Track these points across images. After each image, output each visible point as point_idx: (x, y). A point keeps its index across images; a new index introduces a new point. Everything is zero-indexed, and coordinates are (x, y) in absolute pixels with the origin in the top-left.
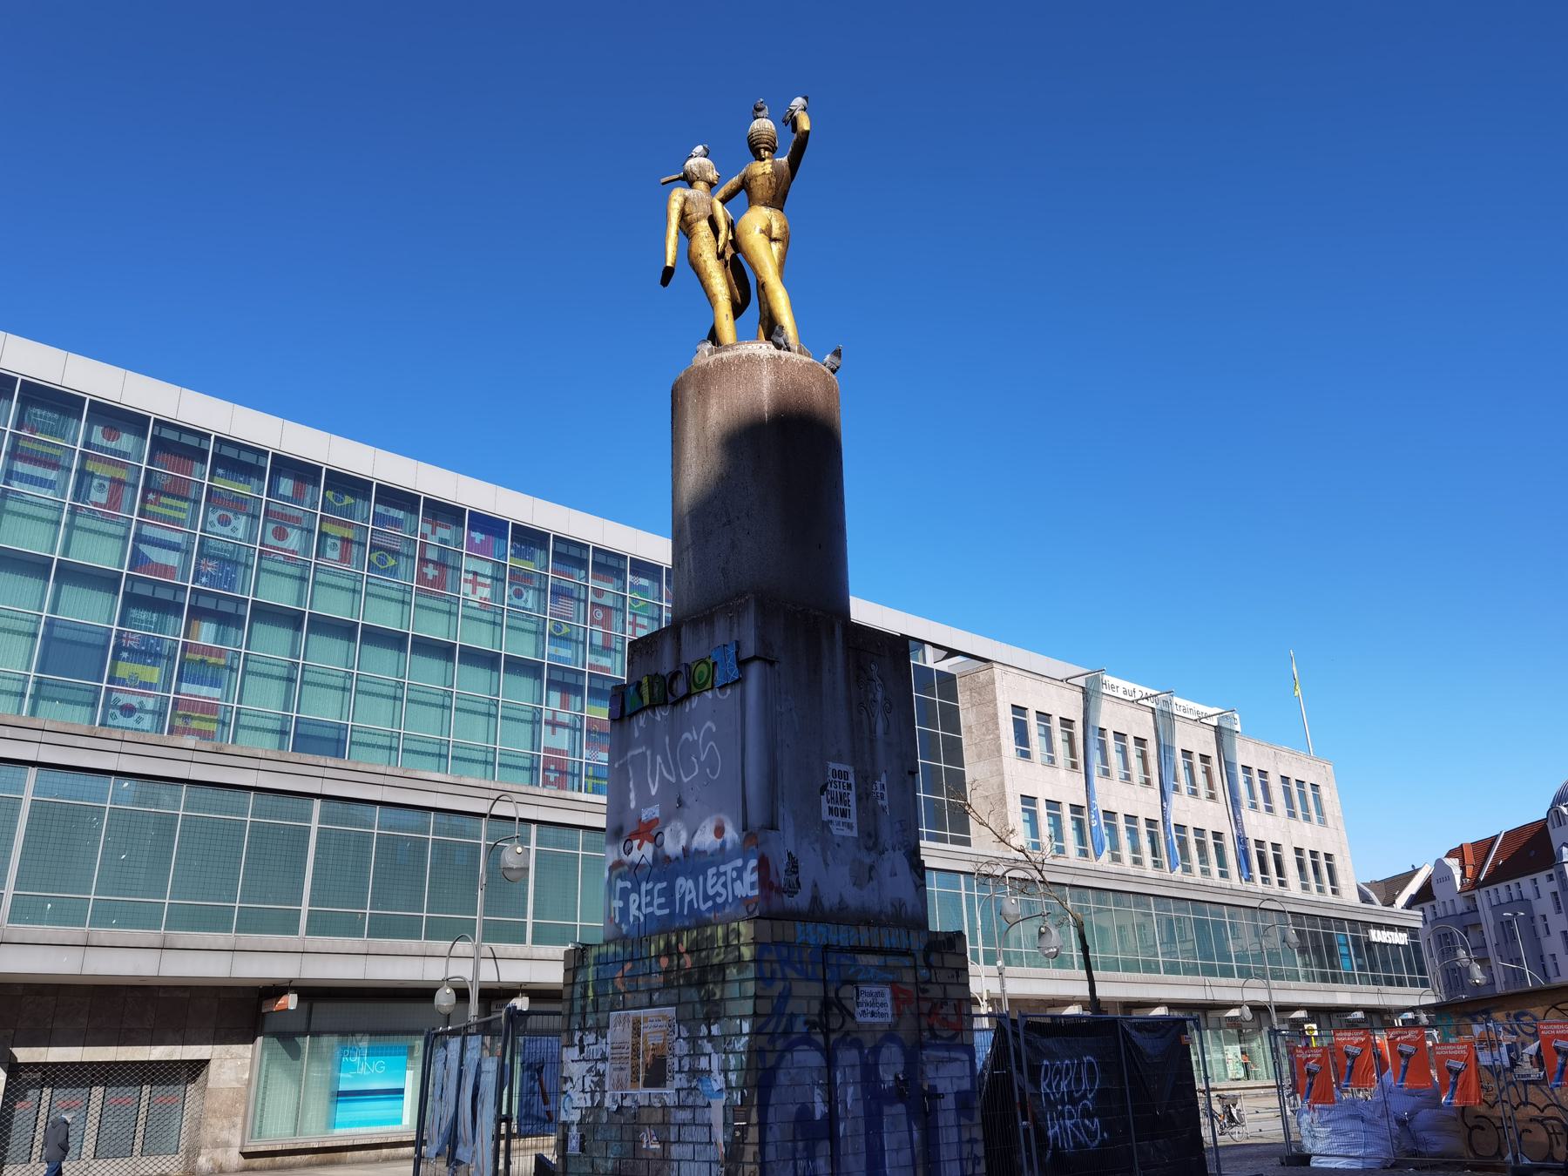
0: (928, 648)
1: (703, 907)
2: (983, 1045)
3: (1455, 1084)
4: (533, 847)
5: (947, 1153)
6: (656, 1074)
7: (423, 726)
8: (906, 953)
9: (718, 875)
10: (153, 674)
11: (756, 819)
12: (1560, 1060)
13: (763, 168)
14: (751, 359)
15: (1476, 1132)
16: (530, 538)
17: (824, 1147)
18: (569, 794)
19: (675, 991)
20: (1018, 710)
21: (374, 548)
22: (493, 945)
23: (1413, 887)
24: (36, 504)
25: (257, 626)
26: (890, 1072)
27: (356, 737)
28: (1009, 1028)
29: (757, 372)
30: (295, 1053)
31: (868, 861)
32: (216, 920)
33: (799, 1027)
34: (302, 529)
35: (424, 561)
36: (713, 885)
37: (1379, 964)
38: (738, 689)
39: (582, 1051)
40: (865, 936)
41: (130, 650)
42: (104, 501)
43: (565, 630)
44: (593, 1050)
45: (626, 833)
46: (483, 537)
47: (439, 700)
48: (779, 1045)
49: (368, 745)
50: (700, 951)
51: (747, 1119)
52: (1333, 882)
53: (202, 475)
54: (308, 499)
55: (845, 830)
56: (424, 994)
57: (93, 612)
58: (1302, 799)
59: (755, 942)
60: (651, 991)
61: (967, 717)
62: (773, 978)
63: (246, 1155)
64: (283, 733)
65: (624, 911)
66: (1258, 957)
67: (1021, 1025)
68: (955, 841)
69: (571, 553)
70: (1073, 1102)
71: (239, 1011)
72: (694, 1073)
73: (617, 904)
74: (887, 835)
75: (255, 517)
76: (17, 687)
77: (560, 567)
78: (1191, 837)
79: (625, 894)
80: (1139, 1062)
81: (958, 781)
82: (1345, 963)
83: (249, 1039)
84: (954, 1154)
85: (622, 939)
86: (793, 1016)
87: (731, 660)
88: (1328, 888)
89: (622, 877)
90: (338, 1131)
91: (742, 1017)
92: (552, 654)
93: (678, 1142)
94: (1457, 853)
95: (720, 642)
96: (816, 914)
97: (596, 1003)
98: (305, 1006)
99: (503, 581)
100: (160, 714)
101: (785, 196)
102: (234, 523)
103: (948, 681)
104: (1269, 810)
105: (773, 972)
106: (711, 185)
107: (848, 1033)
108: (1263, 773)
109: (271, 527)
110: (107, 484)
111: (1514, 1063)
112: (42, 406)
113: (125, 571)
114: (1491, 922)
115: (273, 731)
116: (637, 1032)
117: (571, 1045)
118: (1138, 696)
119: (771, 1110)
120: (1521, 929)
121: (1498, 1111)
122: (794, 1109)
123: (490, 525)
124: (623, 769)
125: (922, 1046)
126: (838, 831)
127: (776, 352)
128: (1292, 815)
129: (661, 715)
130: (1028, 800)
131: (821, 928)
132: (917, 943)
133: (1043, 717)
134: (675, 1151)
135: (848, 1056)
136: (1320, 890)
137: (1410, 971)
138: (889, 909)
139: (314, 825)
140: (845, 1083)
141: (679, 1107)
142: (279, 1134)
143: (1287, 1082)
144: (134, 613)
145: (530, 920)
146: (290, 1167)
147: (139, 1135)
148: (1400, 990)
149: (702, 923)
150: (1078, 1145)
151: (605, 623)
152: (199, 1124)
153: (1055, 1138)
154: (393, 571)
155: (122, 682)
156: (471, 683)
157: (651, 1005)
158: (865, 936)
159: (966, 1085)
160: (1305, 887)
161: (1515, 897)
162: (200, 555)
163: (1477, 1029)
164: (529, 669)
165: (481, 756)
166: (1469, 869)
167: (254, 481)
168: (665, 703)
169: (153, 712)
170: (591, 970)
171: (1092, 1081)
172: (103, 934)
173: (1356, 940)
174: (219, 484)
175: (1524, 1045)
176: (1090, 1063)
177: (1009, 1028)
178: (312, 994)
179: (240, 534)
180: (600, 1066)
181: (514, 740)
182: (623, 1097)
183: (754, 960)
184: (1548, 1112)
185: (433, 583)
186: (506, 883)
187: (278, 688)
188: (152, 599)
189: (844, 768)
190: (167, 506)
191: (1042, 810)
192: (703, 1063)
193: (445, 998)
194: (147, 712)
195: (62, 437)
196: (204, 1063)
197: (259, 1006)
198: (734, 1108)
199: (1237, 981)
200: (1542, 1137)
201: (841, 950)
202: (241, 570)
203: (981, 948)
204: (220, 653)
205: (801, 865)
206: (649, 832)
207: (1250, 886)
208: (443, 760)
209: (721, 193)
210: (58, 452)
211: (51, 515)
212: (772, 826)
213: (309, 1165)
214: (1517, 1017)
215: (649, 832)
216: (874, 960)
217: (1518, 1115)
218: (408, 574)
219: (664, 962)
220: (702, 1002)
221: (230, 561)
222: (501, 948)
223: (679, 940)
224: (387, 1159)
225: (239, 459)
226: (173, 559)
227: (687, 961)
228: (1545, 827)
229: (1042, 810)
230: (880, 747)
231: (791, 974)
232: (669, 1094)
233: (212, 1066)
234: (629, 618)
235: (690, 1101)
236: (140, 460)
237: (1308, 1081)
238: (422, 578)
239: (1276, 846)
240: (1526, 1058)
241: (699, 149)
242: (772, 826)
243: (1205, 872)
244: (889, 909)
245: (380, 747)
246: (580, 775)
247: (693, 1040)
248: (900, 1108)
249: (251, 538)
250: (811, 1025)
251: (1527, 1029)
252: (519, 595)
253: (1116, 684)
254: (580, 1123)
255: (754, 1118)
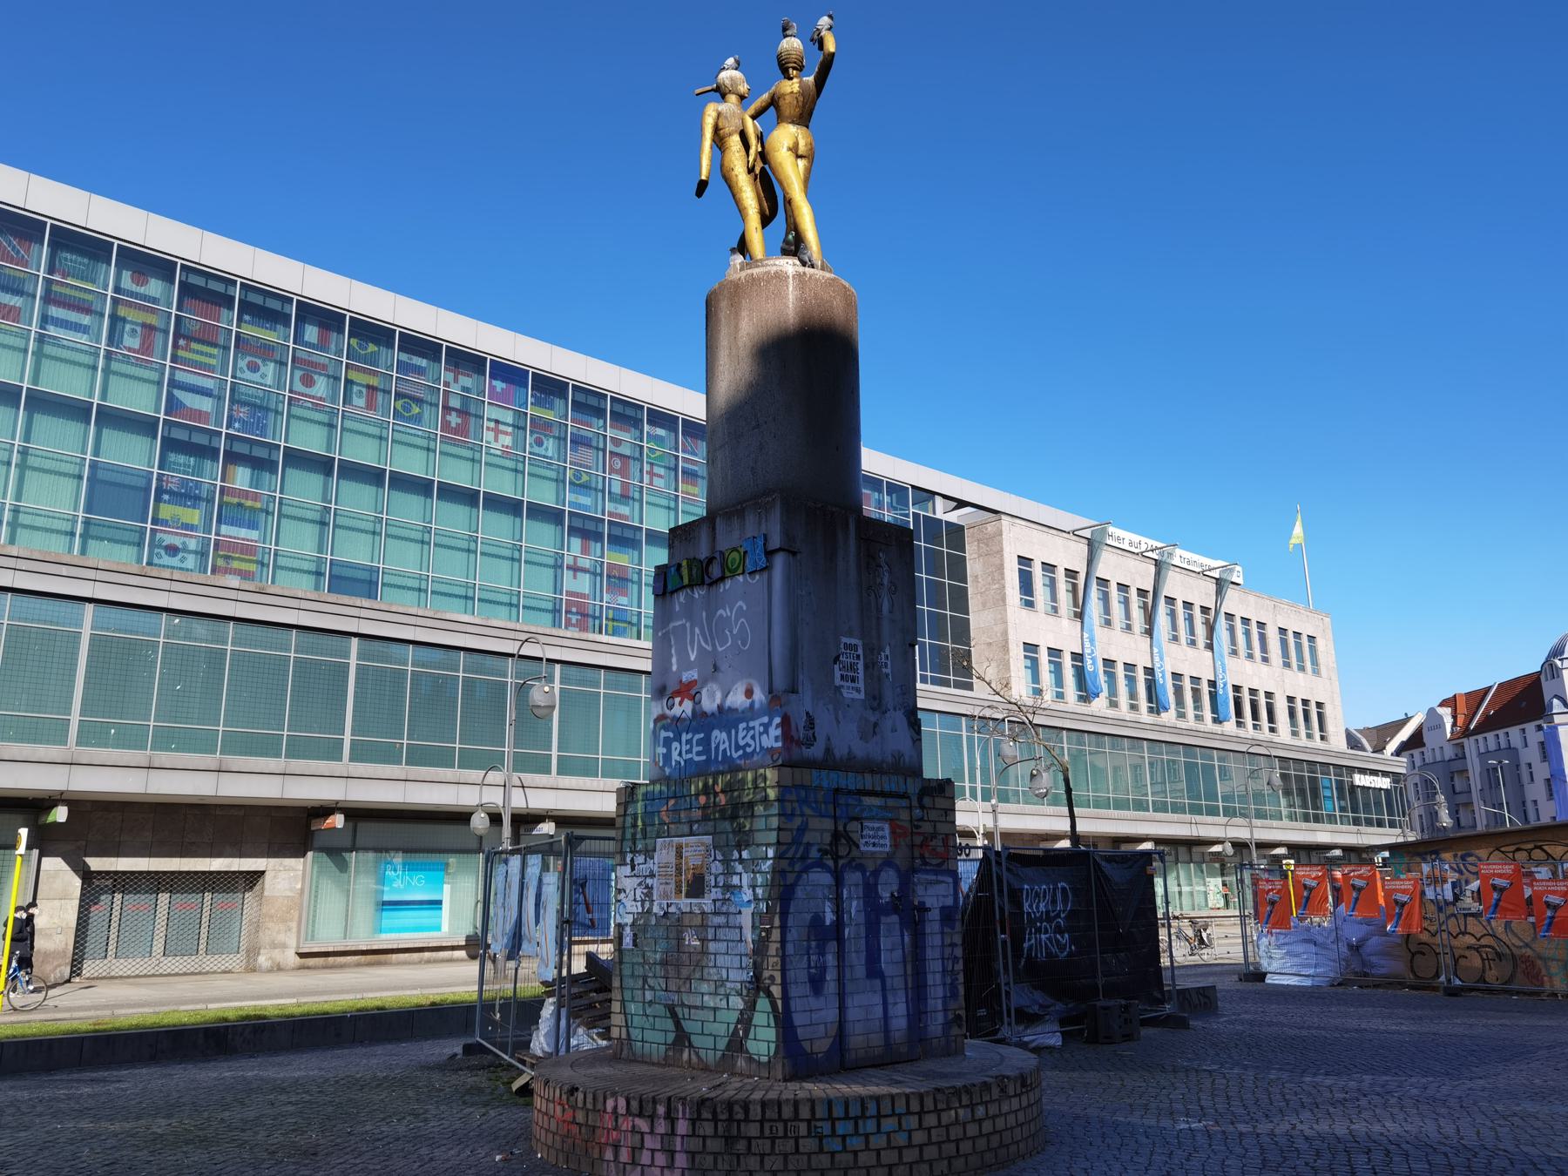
0: (938, 500)
1: (735, 755)
2: (968, 871)
3: (1400, 915)
4: (557, 685)
5: (932, 953)
6: (696, 887)
7: (450, 568)
8: (904, 796)
9: (748, 729)
10: (194, 516)
11: (780, 683)
12: (1495, 895)
13: (791, 87)
14: (780, 277)
15: (1418, 958)
16: (550, 387)
17: (832, 946)
18: (591, 636)
19: (711, 823)
20: (1024, 561)
21: (399, 395)
22: (522, 775)
23: (1404, 734)
24: (73, 349)
25: (289, 471)
26: (887, 888)
27: (387, 579)
28: (993, 858)
29: (784, 289)
30: (343, 867)
31: (873, 719)
32: (267, 747)
33: (814, 853)
34: (328, 377)
35: (447, 409)
36: (743, 737)
37: (1359, 805)
38: (765, 575)
39: (633, 869)
40: (868, 781)
41: (171, 492)
42: (137, 346)
43: (585, 478)
44: (642, 869)
45: (669, 692)
46: (504, 385)
47: (464, 545)
48: (798, 867)
49: (399, 587)
50: (732, 791)
51: (771, 923)
52: (1322, 728)
53: (230, 321)
54: (333, 346)
55: (854, 693)
56: (461, 817)
57: (133, 455)
58: (1298, 650)
59: (779, 785)
60: (691, 823)
61: (973, 567)
62: (793, 815)
63: (302, 955)
64: (319, 574)
65: (667, 757)
66: (1243, 798)
67: (1004, 857)
68: (958, 685)
69: (590, 402)
70: (1049, 920)
71: (292, 828)
72: (728, 887)
73: (661, 750)
74: (889, 697)
75: (283, 364)
76: (66, 526)
77: (579, 416)
78: (1187, 685)
79: (667, 743)
80: (1110, 886)
81: (962, 631)
82: (1329, 804)
83: (303, 855)
84: (937, 954)
85: (667, 780)
86: (809, 845)
87: (759, 550)
88: (1317, 735)
89: (666, 728)
90: (383, 936)
91: (767, 845)
92: (573, 501)
93: (715, 940)
94: (1451, 702)
95: (749, 535)
96: (828, 763)
97: (644, 831)
98: (351, 825)
99: (524, 429)
100: (203, 554)
101: (810, 114)
102: (263, 369)
103: (956, 532)
104: (1265, 660)
105: (793, 809)
106: (742, 97)
107: (853, 859)
108: (1261, 625)
109: (298, 374)
110: (139, 329)
111: (1456, 898)
112: (72, 250)
113: (162, 416)
114: (1478, 769)
115: (309, 572)
116: (679, 855)
117: (624, 864)
118: (1143, 548)
119: (791, 917)
120: (1507, 775)
121: (1438, 940)
122: (808, 917)
123: (510, 373)
124: (666, 637)
125: (915, 871)
126: (848, 694)
127: (801, 269)
128: (1287, 665)
129: (698, 593)
130: (1031, 648)
131: (833, 775)
132: (913, 787)
133: (1049, 567)
134: (712, 946)
135: (853, 878)
136: (1309, 736)
137: (1391, 813)
138: (890, 759)
139: (353, 662)
140: (850, 898)
141: (716, 913)
142: (329, 937)
143: (1250, 910)
144: (172, 457)
145: (554, 753)
146: (342, 966)
147: (204, 936)
148: (1381, 830)
149: (734, 769)
150: (1049, 954)
151: (623, 472)
152: (257, 927)
153: (1030, 948)
154: (418, 419)
155: (165, 523)
156: (495, 528)
157: (692, 834)
158: (868, 781)
159: (950, 902)
160: (1295, 734)
161: (1503, 745)
162: (232, 401)
163: (1426, 868)
164: (551, 516)
165: (505, 599)
166: (1461, 719)
167: (280, 327)
168: (703, 583)
169: (196, 552)
170: (640, 805)
171: (1065, 901)
172: (163, 758)
173: (1340, 785)
174: (247, 330)
175: (1467, 882)
176: (1064, 889)
177: (993, 858)
178: (358, 814)
179: (269, 381)
180: (649, 881)
181: (539, 585)
182: (669, 905)
183: (778, 800)
184: (1483, 942)
185: (456, 431)
186: (532, 719)
187: (311, 531)
188: (186, 444)
189: (853, 641)
190: (197, 352)
191: (1044, 657)
192: (735, 880)
193: (480, 822)
194: (190, 552)
195: (93, 282)
196: (258, 875)
197: (308, 825)
198: (761, 914)
199: (1222, 819)
200: (1477, 962)
201: (850, 792)
202: (271, 416)
203: (979, 786)
204: (256, 497)
205: (817, 722)
206: (688, 691)
207: (1241, 732)
208: (470, 603)
209: (752, 110)
210: (89, 297)
211: (87, 359)
212: (793, 690)
213: (358, 965)
214: (1463, 858)
215: (688, 691)
216: (876, 801)
217: (1455, 943)
218: (432, 423)
219: (702, 799)
220: (734, 832)
221: (261, 408)
222: (529, 778)
223: (715, 782)
224: (429, 961)
225: (265, 305)
226: (206, 404)
227: (722, 799)
228: (1539, 679)
229: (1044, 657)
230: (886, 625)
231: (808, 811)
232: (706, 903)
233: (268, 876)
234: (646, 467)
235: (724, 909)
236: (169, 305)
237: (1269, 911)
238: (446, 426)
239: (1269, 695)
240: (1468, 893)
241: (730, 61)
242: (793, 690)
243: (1199, 718)
244: (890, 759)
245: (409, 589)
246: (601, 617)
247: (726, 862)
248: (895, 918)
249: (280, 384)
250: (824, 852)
251: (1471, 868)
252: (539, 443)
253: (1119, 535)
254: (633, 925)
255: (777, 922)
